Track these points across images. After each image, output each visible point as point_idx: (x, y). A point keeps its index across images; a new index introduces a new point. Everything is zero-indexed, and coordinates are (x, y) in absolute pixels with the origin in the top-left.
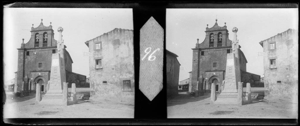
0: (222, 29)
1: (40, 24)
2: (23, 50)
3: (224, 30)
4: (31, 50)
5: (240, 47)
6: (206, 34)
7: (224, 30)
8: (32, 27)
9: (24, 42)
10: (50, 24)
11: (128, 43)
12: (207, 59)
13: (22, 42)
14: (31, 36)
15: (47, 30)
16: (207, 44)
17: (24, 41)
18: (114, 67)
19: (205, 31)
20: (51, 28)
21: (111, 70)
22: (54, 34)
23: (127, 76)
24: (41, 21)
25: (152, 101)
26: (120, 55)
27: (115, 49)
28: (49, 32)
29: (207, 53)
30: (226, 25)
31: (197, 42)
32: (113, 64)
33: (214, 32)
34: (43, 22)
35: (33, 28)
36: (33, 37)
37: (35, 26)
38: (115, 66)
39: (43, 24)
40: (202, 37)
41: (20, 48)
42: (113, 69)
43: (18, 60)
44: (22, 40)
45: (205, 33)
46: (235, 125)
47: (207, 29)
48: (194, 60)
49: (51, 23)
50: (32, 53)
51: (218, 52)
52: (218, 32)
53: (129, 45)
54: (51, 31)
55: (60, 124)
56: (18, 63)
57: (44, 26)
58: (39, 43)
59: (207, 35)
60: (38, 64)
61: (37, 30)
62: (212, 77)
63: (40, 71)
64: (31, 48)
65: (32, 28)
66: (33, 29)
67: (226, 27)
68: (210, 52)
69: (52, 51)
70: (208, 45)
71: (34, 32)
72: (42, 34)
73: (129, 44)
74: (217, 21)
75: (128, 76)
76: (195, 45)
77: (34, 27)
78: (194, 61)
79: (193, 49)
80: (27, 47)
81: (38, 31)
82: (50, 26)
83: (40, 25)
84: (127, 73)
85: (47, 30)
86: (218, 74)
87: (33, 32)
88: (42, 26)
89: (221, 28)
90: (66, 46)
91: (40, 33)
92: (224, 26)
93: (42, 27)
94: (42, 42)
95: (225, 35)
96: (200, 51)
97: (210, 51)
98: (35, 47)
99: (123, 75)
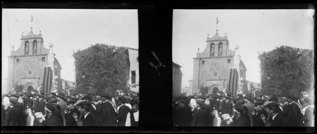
0: (37, 37)
2: (199, 60)
4: (207, 59)
5: (54, 55)
6: (21, 41)
8: (207, 37)
9: (14, 49)
10: (39, 33)
14: (207, 45)
15: (223, 40)
17: (14, 48)
20: (226, 39)
22: (228, 43)
24: (31, 29)
28: (38, 40)
29: (208, 62)
30: (41, 33)
31: (198, 51)
33: (214, 42)
34: (33, 30)
35: (22, 36)
37: (25, 34)
39: (33, 32)
40: (203, 47)
41: (195, 57)
43: (194, 69)
44: (198, 50)
46: (202, 133)
48: (195, 69)
49: (40, 32)
50: (22, 61)
51: (218, 61)
52: (33, 40)
54: (40, 39)
55: (111, 132)
56: (194, 72)
57: (219, 36)
59: (208, 45)
61: (27, 38)
62: (213, 85)
63: (30, 78)
64: (206, 57)
65: (207, 38)
66: (23, 37)
68: (26, 59)
69: (227, 61)
70: (209, 55)
71: (24, 40)
76: (196, 55)
77: (24, 35)
78: (195, 71)
79: (194, 59)
81: (213, 41)
82: (40, 34)
85: (223, 40)
86: (219, 83)
87: (23, 40)
88: (217, 37)
89: (221, 38)
90: (55, 54)
91: (29, 41)
93: (217, 37)
95: (40, 43)
96: (201, 60)
97: (25, 59)
98: (210, 56)
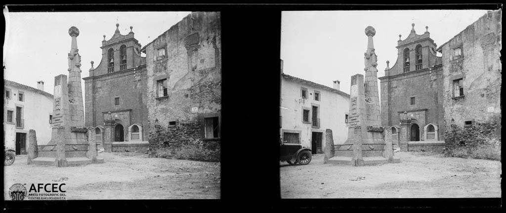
1: (114, 33)
3: (129, 40)
7: (129, 40)
11: (214, 39)
12: (106, 93)
13: (90, 67)
16: (105, 70)
18: (188, 93)
19: (101, 48)
21: (184, 98)
23: (211, 109)
25: (227, 181)
26: (200, 67)
27: (190, 55)
32: (188, 85)
36: (104, 56)
38: (190, 90)
42: (187, 96)
45: (101, 50)
47: (104, 43)
53: (217, 43)
58: (127, 62)
60: (114, 99)
67: (132, 34)
70: (107, 70)
72: (119, 49)
73: (217, 38)
74: (119, 27)
75: (214, 109)
80: (97, 73)
81: (112, 45)
83: (114, 35)
84: (212, 102)
87: (104, 49)
92: (129, 33)
94: (119, 62)
99: (204, 108)
